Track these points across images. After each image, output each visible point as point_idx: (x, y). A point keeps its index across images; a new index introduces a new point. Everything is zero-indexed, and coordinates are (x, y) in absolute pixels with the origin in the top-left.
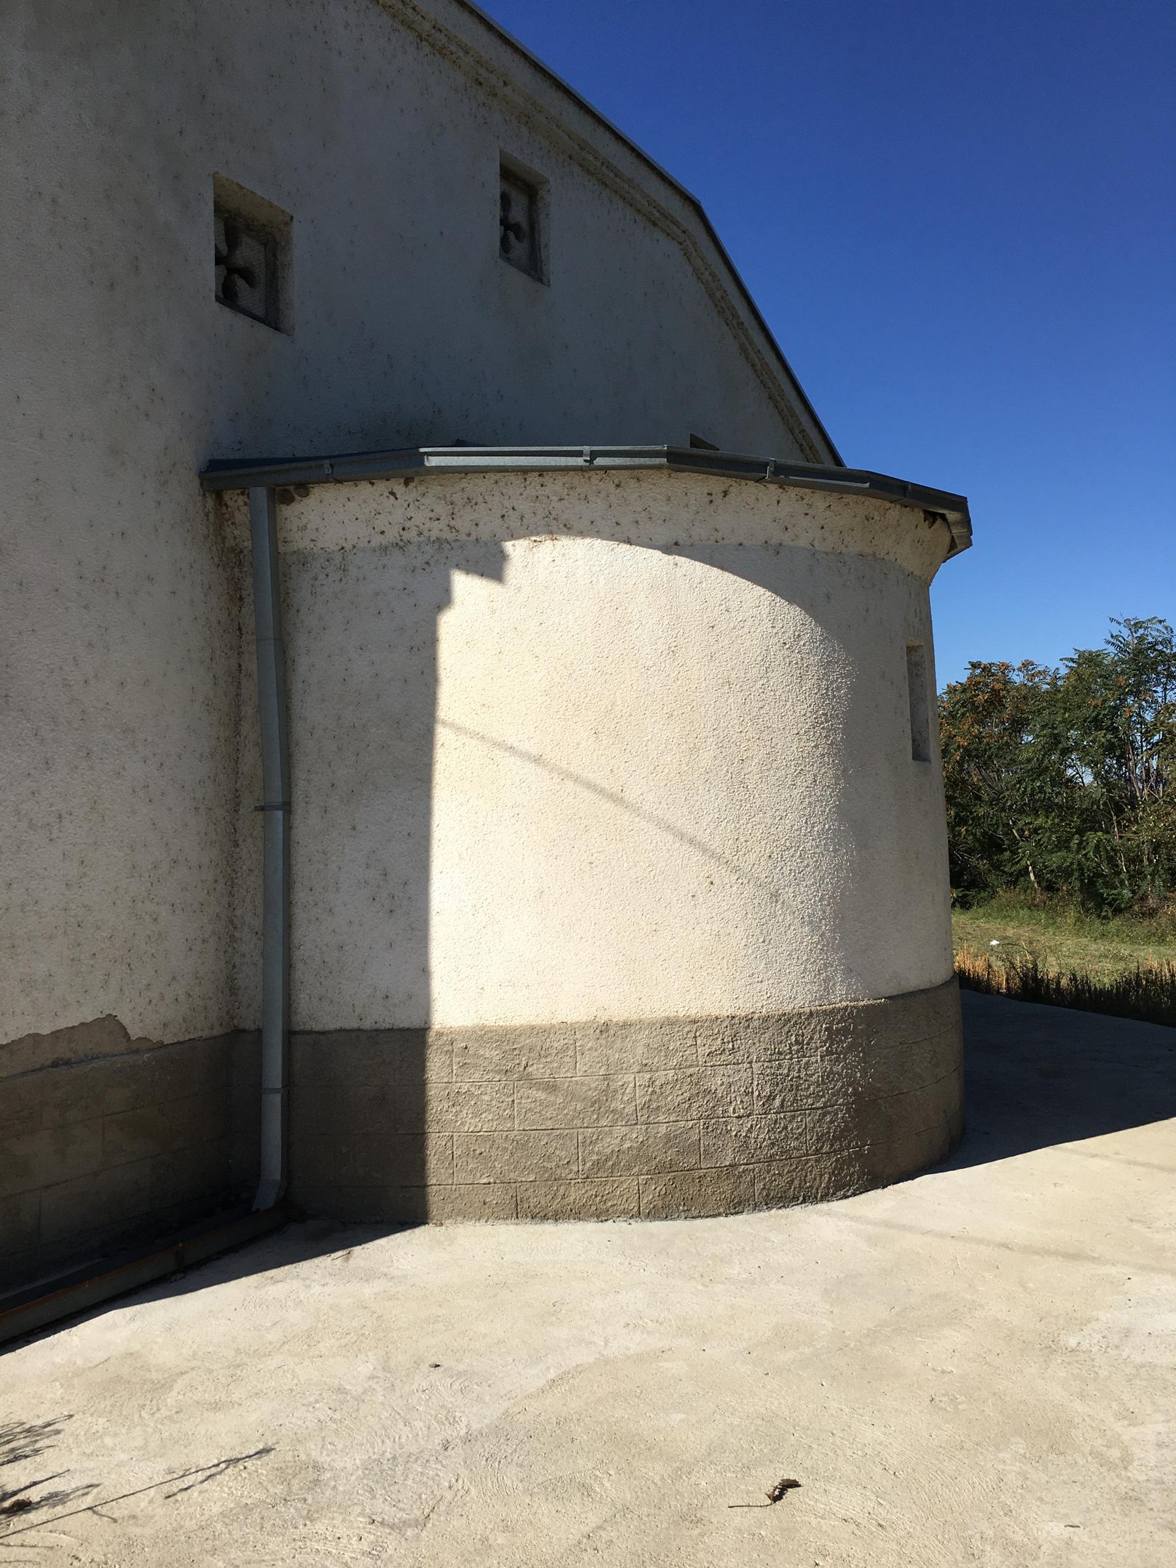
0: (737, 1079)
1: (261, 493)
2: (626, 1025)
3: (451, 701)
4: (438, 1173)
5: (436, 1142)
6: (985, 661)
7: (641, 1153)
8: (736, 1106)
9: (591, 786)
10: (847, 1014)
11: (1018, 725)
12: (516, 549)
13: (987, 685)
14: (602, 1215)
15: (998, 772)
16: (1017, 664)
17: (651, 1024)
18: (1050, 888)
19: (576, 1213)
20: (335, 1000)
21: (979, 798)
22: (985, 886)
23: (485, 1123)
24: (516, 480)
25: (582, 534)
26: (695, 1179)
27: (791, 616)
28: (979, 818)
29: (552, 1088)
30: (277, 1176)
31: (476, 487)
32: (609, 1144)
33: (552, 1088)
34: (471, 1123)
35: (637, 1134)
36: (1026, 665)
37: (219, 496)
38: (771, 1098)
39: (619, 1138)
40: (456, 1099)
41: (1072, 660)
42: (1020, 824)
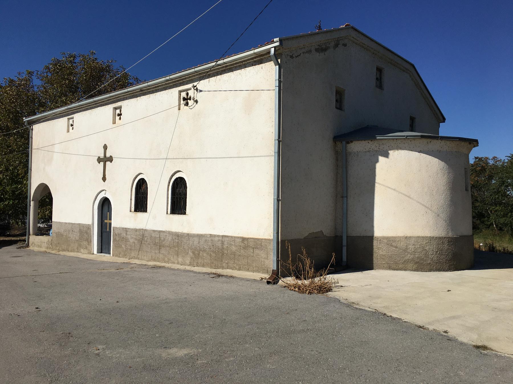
0: (431, 248)
1: (344, 142)
2: (410, 237)
3: (379, 178)
4: (375, 261)
5: (375, 255)
6: (480, 156)
7: (413, 260)
8: (431, 253)
9: (404, 194)
10: (452, 238)
11: (491, 177)
12: (391, 152)
13: (480, 164)
14: (405, 270)
15: (484, 192)
16: (491, 158)
17: (415, 237)
18: (501, 229)
19: (401, 269)
20: (356, 230)
21: (477, 200)
22: (478, 229)
23: (384, 253)
24: (392, 140)
25: (403, 150)
26: (422, 265)
27: (442, 164)
28: (476, 207)
29: (396, 247)
30: (346, 260)
31: (383, 142)
32: (407, 258)
33: (396, 247)
34: (381, 253)
35: (412, 256)
36: (494, 158)
37: (335, 143)
38: (437, 252)
39: (409, 257)
40: (378, 249)
41: (509, 157)
42: (491, 209)
